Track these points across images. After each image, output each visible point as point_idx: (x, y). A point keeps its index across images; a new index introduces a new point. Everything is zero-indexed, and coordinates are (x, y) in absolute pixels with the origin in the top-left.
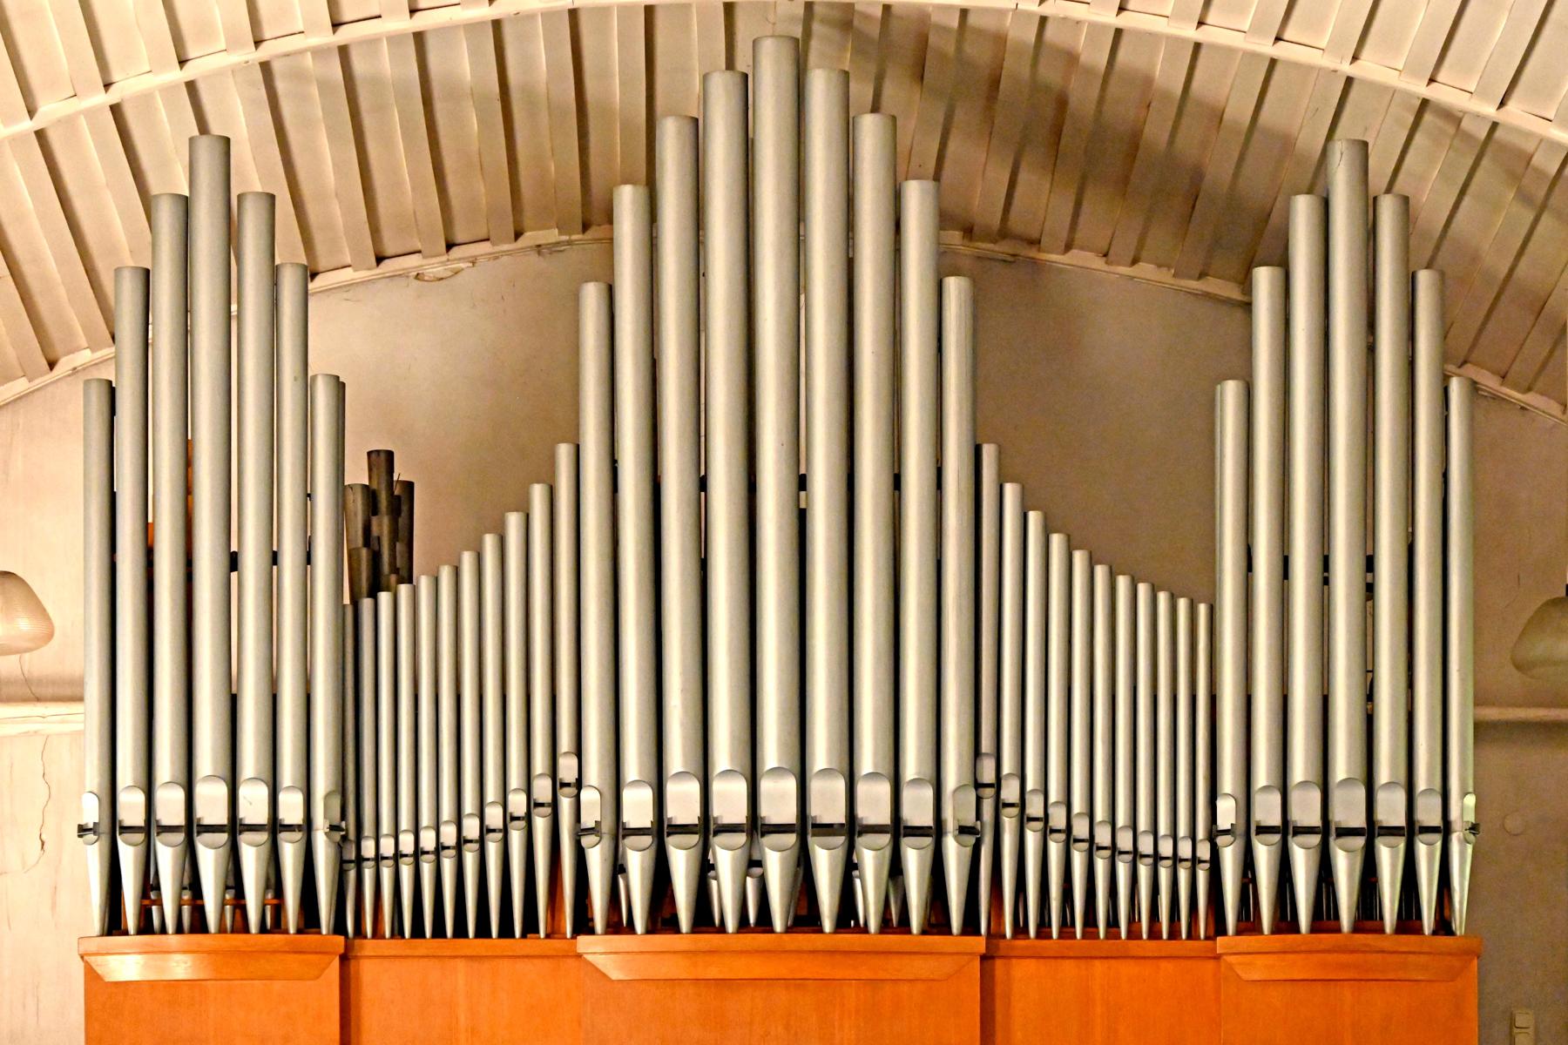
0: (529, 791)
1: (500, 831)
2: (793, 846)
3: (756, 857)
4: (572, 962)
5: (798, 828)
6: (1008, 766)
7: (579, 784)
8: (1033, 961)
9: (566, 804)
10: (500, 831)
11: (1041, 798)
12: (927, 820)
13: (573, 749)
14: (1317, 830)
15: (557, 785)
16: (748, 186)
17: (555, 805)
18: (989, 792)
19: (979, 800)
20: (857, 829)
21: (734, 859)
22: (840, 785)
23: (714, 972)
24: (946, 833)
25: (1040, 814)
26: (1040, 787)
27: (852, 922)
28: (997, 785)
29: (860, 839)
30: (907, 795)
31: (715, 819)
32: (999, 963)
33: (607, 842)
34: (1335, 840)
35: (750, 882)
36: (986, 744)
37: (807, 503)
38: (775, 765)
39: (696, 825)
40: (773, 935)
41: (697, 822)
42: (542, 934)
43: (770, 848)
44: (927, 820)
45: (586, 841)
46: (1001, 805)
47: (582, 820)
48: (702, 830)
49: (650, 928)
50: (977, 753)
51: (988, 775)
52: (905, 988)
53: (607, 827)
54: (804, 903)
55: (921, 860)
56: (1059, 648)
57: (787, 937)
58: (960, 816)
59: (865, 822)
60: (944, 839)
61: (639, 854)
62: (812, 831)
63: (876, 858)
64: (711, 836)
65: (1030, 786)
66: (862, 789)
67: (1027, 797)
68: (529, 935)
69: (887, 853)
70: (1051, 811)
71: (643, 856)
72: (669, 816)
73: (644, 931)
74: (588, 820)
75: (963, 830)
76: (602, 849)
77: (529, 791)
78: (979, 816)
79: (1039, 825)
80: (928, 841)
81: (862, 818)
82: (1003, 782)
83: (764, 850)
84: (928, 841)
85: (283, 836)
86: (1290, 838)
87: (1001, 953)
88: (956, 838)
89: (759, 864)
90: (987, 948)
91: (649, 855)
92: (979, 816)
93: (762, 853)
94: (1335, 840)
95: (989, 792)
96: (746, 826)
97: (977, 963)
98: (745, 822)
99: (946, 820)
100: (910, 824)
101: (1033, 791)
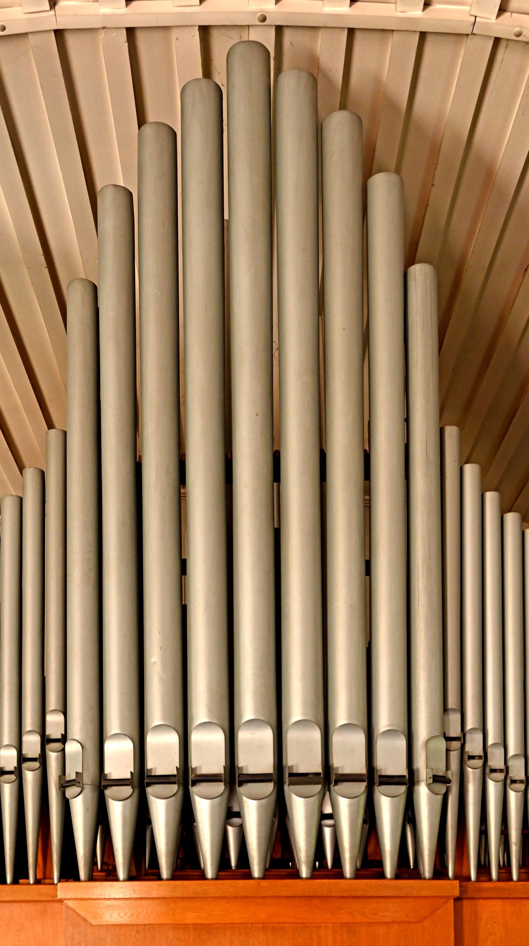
0: (19, 748)
1: (480, 757)
2: (363, 793)
3: (236, 809)
4: (57, 905)
5: (275, 777)
6: (470, 724)
7: (64, 739)
8: (499, 901)
9: (53, 757)
10: (480, 757)
11: (502, 751)
12: (401, 770)
13: (60, 708)
14: (402, 780)
15: (45, 740)
16: (271, 204)
17: (43, 759)
18: (456, 745)
19: (448, 751)
20: (333, 778)
21: (212, 808)
22: (360, 738)
23: (191, 918)
24: (418, 782)
25: (501, 766)
26: (500, 740)
27: (290, 864)
28: (462, 739)
29: (336, 787)
30: (380, 745)
31: (194, 770)
32: (465, 903)
33: (89, 793)
34: (334, 786)
35: (231, 831)
36: (453, 701)
37: (404, 423)
38: (252, 717)
39: (174, 776)
40: (251, 881)
41: (175, 773)
42: (31, 881)
43: (247, 797)
44: (401, 770)
45: (70, 792)
46: (466, 757)
47: (67, 773)
48: (181, 781)
49: (156, 877)
50: (445, 710)
51: (455, 731)
52: (382, 931)
53: (88, 778)
54: (279, 848)
55: (394, 808)
56: (211, 691)
57: (265, 883)
58: (433, 765)
59: (340, 772)
60: (416, 788)
61: (164, 801)
62: (289, 780)
63: (350, 805)
64: (190, 787)
65: (491, 740)
66: (336, 739)
67: (489, 750)
68: (21, 881)
69: (362, 800)
70: (510, 763)
71: (124, 806)
72: (193, 766)
73: (126, 877)
74: (71, 775)
75: (437, 779)
76: (84, 799)
77: (19, 748)
78: (448, 768)
79: (501, 776)
80: (402, 789)
81: (337, 768)
82: (468, 736)
83: (242, 799)
84: (402, 789)
85: (379, 790)
86: (286, 787)
87: (470, 895)
88: (428, 786)
89: (238, 815)
90: (460, 891)
91: (132, 803)
92: (448, 768)
93: (241, 804)
94: (289, 785)
95: (456, 745)
96: (223, 776)
97: (451, 905)
98: (222, 771)
99: (418, 770)
100: (384, 773)
101: (494, 745)
